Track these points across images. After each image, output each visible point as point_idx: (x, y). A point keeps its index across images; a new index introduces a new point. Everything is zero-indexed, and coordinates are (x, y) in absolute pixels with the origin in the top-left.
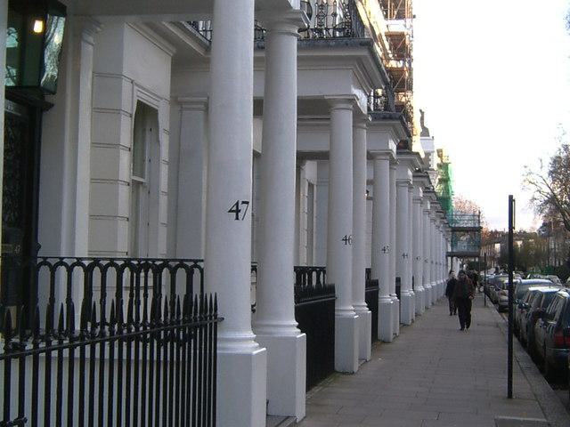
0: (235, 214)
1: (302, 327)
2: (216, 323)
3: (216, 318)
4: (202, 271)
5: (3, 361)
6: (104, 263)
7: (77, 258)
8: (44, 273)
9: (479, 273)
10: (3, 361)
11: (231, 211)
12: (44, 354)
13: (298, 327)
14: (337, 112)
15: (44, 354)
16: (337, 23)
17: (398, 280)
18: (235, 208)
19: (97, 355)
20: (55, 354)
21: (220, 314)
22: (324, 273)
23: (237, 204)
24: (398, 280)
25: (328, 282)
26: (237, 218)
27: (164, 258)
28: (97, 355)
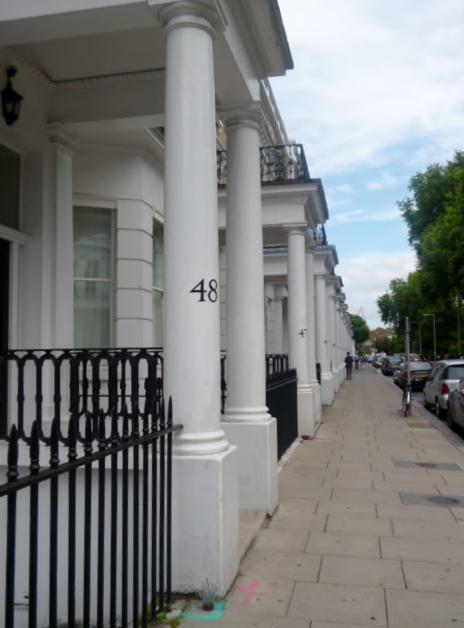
0: (199, 294)
1: (272, 412)
2: (170, 435)
3: (170, 425)
4: (162, 360)
5: (5, 498)
6: (39, 355)
7: (45, 350)
8: (13, 366)
9: (449, 305)
10: (5, 498)
11: (193, 291)
12: (83, 467)
13: (269, 412)
14: (294, 236)
15: (83, 467)
16: (426, 422)
17: (318, 366)
18: (199, 288)
19: (120, 466)
20: (95, 465)
21: (175, 421)
22: (287, 359)
23: (202, 283)
24: (318, 366)
25: (291, 367)
26: (202, 299)
27: (47, 348)
28: (120, 466)
